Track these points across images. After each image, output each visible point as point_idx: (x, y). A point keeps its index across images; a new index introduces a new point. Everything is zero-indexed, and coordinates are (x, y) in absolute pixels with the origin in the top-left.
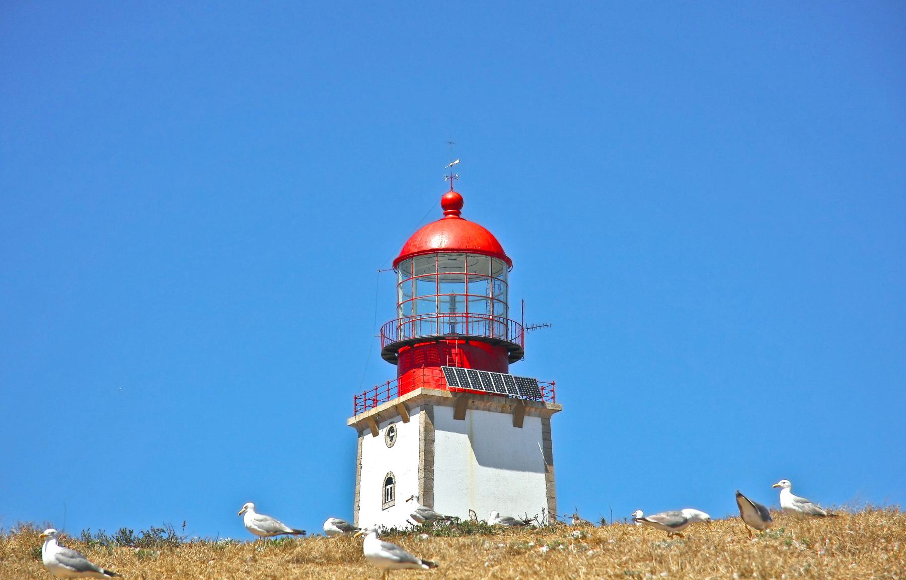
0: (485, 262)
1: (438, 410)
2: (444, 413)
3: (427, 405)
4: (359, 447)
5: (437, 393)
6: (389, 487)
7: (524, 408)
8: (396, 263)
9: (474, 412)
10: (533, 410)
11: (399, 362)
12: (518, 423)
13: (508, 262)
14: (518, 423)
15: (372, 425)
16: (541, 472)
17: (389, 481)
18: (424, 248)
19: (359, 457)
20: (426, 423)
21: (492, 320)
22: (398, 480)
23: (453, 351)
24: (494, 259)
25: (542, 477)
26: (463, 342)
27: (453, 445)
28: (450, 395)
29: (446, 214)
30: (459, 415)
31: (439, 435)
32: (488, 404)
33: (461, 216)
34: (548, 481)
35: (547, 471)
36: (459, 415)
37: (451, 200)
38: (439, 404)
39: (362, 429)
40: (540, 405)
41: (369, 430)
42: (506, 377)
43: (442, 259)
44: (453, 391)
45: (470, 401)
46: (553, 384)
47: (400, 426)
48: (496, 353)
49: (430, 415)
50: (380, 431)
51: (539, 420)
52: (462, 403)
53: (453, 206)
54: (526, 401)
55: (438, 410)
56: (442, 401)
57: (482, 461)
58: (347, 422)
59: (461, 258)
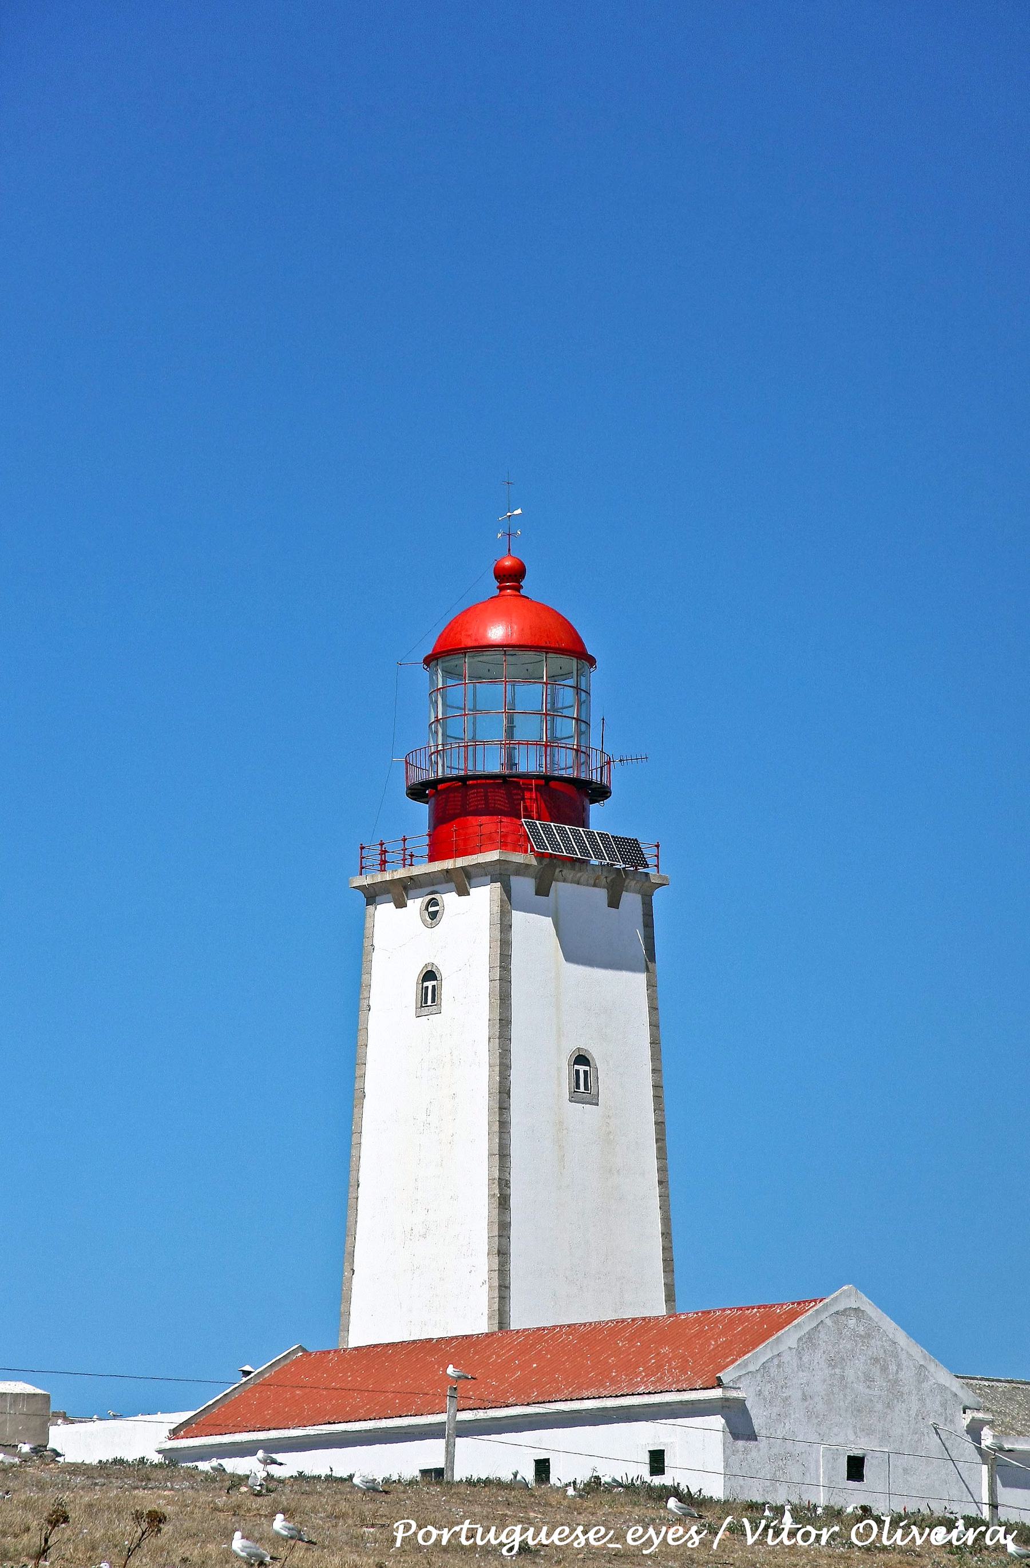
0: (548, 665)
1: (516, 882)
2: (523, 885)
3: (500, 874)
4: (368, 920)
5: (518, 858)
6: (429, 984)
7: (625, 880)
8: (428, 661)
9: (561, 885)
10: (633, 883)
11: (433, 800)
12: (614, 902)
13: (591, 661)
14: (614, 902)
15: (399, 892)
16: (639, 971)
17: (430, 975)
18: (484, 642)
19: (367, 932)
20: (502, 901)
21: (577, 751)
22: (445, 971)
23: (527, 795)
24: (550, 655)
25: (641, 978)
26: (543, 782)
27: (535, 931)
28: (534, 862)
29: (501, 589)
30: (542, 890)
31: (518, 917)
32: (579, 875)
33: (523, 592)
34: (651, 985)
35: (647, 970)
36: (542, 890)
37: (510, 568)
38: (517, 873)
39: (372, 895)
40: (643, 876)
41: (390, 895)
42: (587, 833)
43: (497, 656)
44: (540, 856)
45: (558, 870)
46: (658, 846)
47: (450, 900)
48: (570, 797)
49: (507, 890)
50: (409, 902)
51: (639, 897)
52: (549, 872)
53: (511, 577)
54: (625, 870)
55: (516, 882)
56: (522, 870)
57: (569, 958)
58: (349, 882)
59: (530, 656)
